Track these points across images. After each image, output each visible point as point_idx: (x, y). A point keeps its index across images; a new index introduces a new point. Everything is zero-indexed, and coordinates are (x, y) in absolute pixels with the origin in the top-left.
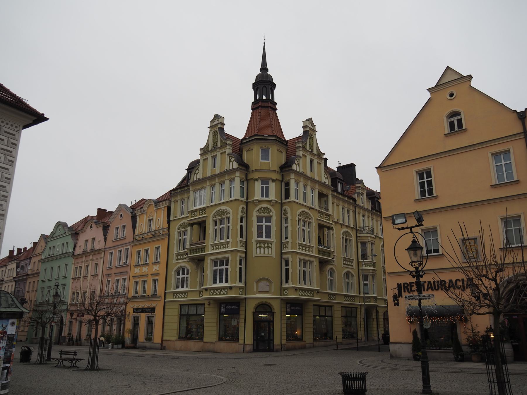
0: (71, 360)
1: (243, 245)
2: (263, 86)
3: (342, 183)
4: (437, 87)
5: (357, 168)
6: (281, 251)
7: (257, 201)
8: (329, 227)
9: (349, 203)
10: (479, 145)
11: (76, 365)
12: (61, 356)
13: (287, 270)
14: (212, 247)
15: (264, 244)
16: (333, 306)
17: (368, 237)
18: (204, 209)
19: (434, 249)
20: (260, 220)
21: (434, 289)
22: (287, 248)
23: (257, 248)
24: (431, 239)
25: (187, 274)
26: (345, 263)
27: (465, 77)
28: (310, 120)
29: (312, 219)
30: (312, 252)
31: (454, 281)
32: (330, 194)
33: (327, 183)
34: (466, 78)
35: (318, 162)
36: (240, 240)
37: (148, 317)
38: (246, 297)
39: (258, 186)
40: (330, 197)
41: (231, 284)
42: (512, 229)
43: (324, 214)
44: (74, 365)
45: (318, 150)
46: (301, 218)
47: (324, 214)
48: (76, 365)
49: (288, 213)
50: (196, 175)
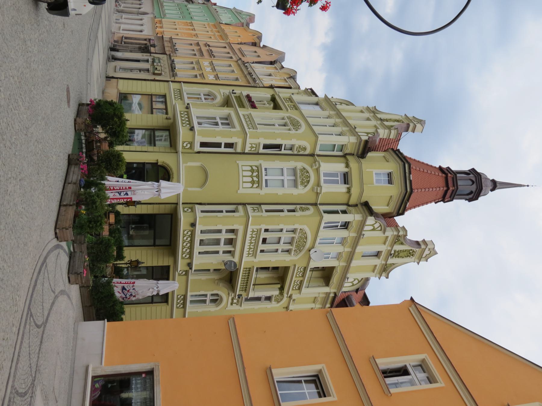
1: (253, 149)
2: (474, 179)
6: (249, 204)
8: (283, 289)
15: (258, 176)
16: (168, 304)
23: (251, 166)
29: (296, 256)
32: (331, 290)
33: (346, 285)
35: (376, 266)
38: (179, 153)
39: (339, 167)
40: (326, 289)
41: (197, 130)
45: (394, 266)
46: (297, 234)
49: (303, 212)
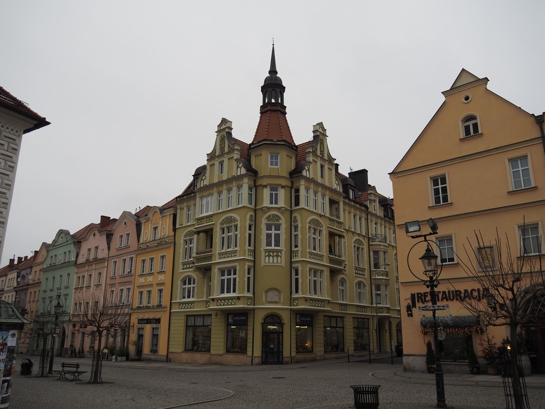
0: (73, 373)
1: (252, 254)
2: (272, 89)
3: (354, 189)
4: (452, 90)
5: (369, 174)
6: (291, 259)
7: (266, 208)
8: (341, 235)
9: (361, 211)
10: (495, 150)
11: (78, 378)
12: (63, 368)
13: (297, 280)
14: (219, 256)
15: (273, 252)
16: (345, 317)
17: (380, 245)
18: (211, 216)
19: (449, 257)
20: (269, 227)
21: (449, 300)
22: (297, 257)
23: (266, 257)
24: (446, 247)
25: (194, 283)
26: (357, 272)
27: (481, 80)
28: (321, 125)
29: (323, 227)
30: (322, 261)
31: (469, 291)
32: (341, 201)
33: (338, 190)
34: (482, 81)
35: (328, 168)
36: (248, 249)
37: (153, 329)
38: (255, 308)
39: (266, 192)
40: (341, 204)
41: (239, 294)
42: (530, 237)
43: (335, 222)
44: (76, 378)
45: (329, 155)
46: (312, 226)
47: (335, 222)
48: (78, 378)
49: (298, 221)
50: (202, 181)
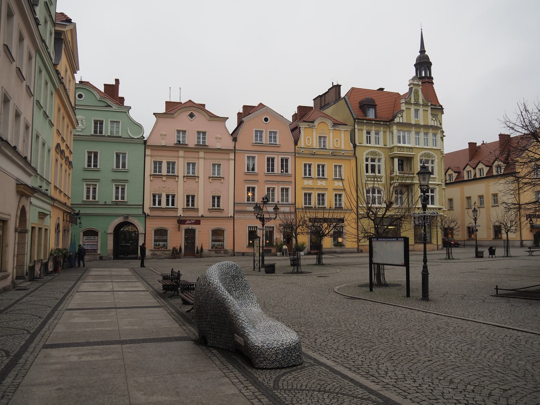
18: (412, 148)
33: (436, 125)
